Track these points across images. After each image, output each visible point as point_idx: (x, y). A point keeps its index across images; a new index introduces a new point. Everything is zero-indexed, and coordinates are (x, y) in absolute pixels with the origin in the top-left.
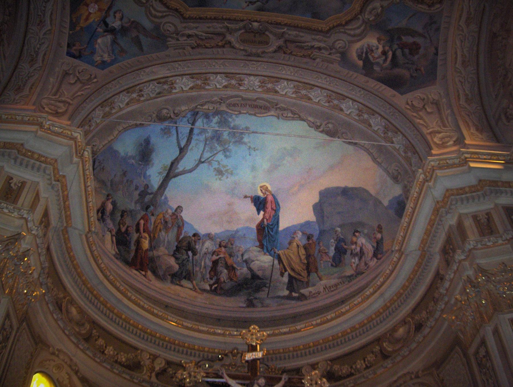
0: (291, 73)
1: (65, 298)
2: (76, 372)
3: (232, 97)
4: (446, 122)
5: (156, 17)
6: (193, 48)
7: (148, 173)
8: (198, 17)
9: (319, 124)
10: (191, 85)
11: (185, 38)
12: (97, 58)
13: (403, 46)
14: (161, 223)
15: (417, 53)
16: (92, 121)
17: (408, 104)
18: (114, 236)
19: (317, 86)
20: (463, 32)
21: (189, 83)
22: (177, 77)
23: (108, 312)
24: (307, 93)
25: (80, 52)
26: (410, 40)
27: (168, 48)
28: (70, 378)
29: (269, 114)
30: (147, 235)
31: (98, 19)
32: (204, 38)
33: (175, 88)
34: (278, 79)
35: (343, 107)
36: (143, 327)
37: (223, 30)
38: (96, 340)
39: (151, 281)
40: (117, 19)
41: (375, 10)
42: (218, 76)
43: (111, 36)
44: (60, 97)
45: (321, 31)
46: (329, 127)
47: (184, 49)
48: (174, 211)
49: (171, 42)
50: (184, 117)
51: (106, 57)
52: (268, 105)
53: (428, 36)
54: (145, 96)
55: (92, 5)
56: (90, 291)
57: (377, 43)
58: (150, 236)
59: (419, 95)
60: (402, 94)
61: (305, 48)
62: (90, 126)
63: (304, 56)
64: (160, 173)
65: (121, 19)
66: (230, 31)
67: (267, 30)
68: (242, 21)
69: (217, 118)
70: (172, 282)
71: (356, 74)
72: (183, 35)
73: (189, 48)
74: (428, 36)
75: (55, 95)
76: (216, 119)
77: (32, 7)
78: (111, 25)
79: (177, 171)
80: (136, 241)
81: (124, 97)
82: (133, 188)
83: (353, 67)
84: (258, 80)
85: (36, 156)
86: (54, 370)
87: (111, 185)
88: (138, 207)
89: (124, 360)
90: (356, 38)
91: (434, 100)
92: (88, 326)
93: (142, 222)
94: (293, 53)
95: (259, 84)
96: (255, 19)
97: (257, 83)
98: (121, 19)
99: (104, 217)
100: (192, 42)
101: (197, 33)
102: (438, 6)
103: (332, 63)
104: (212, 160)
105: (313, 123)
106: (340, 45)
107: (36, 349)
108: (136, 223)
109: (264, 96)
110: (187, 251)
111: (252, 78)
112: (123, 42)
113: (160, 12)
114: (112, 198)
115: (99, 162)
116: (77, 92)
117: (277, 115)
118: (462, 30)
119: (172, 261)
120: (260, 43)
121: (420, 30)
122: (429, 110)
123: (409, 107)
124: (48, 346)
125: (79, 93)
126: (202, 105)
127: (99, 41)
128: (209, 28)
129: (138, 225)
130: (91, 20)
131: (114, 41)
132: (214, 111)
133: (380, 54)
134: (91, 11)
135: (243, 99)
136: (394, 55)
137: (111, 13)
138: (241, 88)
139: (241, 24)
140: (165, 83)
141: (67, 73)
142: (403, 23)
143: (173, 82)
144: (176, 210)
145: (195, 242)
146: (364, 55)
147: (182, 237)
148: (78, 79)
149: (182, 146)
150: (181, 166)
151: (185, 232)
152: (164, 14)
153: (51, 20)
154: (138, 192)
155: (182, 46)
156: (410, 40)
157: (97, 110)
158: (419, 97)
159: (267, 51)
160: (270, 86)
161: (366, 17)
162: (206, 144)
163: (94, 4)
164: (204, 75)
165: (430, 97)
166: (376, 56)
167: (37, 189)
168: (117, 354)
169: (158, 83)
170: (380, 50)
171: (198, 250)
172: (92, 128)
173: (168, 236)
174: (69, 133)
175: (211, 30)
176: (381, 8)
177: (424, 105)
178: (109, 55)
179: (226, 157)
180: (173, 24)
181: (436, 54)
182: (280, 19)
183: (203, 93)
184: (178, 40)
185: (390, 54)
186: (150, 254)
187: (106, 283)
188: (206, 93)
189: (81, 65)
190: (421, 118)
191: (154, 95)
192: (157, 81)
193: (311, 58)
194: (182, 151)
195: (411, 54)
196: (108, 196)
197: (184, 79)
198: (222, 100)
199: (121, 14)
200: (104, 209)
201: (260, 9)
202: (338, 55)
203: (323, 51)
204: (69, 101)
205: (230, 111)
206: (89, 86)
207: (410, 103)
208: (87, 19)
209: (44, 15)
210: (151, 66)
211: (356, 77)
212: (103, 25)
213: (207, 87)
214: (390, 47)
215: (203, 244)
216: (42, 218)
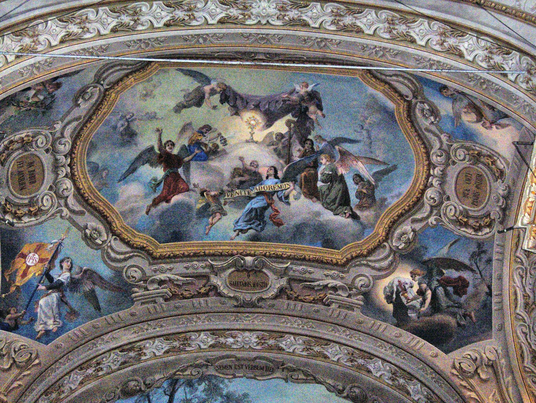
0: (299, 325)
3: (223, 357)
4: (506, 395)
5: (119, 261)
6: (166, 300)
8: (172, 255)
9: (341, 388)
10: (167, 348)
11: (156, 286)
12: (39, 327)
13: (445, 283)
15: (465, 293)
17: (454, 367)
19: (334, 342)
20: (523, 265)
24: (322, 350)
26: (453, 274)
27: (133, 302)
31: (40, 272)
33: (145, 354)
34: (282, 334)
35: (371, 367)
37: (207, 270)
41: (405, 236)
42: (202, 335)
43: (57, 294)
45: (337, 264)
46: (355, 392)
47: (155, 302)
49: (139, 292)
50: (158, 388)
51: (51, 326)
53: (476, 269)
54: (105, 369)
55: (31, 255)
57: (411, 278)
59: (469, 353)
60: (447, 352)
61: (316, 289)
63: (314, 301)
65: (70, 270)
66: (216, 272)
67: (264, 265)
68: (232, 255)
69: (204, 384)
71: (384, 325)
72: (153, 282)
73: (161, 300)
74: (476, 269)
76: (202, 386)
78: (56, 278)
81: (76, 376)
83: (379, 312)
84: (255, 336)
90: (383, 273)
91: (489, 360)
94: (300, 298)
95: (257, 340)
96: (248, 252)
97: (254, 339)
98: (70, 270)
100: (165, 290)
101: (172, 276)
102: (487, 230)
103: (353, 310)
105: (334, 387)
106: (362, 283)
109: (266, 354)
111: (247, 334)
113: (121, 253)
116: (13, 382)
117: (285, 377)
118: (522, 263)
120: (255, 285)
121: (467, 262)
122: (483, 376)
123: (455, 372)
125: (16, 384)
126: (182, 371)
127: (42, 302)
128: (187, 268)
130: (30, 276)
131: (62, 300)
133: (416, 294)
134: (29, 264)
135: (238, 359)
136: (434, 296)
137: (57, 262)
139: (230, 260)
140: (130, 350)
142: (443, 252)
146: (394, 296)
148: (14, 361)
155: (152, 297)
156: (453, 274)
158: (469, 357)
159: (265, 297)
160: (271, 342)
161: (394, 244)
163: (33, 254)
164: (183, 335)
165: (484, 356)
166: (410, 296)
169: (121, 351)
170: (416, 288)
175: (190, 271)
176: (412, 233)
177: (477, 368)
181: (490, 294)
182: (280, 251)
184: (146, 289)
185: (429, 294)
190: (472, 389)
192: (120, 349)
193: (324, 304)
195: (456, 292)
197: (156, 341)
198: (209, 362)
199: (69, 263)
201: (255, 238)
202: (361, 297)
203: (340, 292)
205: (221, 375)
206: (29, 372)
207: (457, 366)
208: (25, 274)
210: (111, 331)
211: (385, 328)
213: (188, 349)
214: (429, 285)
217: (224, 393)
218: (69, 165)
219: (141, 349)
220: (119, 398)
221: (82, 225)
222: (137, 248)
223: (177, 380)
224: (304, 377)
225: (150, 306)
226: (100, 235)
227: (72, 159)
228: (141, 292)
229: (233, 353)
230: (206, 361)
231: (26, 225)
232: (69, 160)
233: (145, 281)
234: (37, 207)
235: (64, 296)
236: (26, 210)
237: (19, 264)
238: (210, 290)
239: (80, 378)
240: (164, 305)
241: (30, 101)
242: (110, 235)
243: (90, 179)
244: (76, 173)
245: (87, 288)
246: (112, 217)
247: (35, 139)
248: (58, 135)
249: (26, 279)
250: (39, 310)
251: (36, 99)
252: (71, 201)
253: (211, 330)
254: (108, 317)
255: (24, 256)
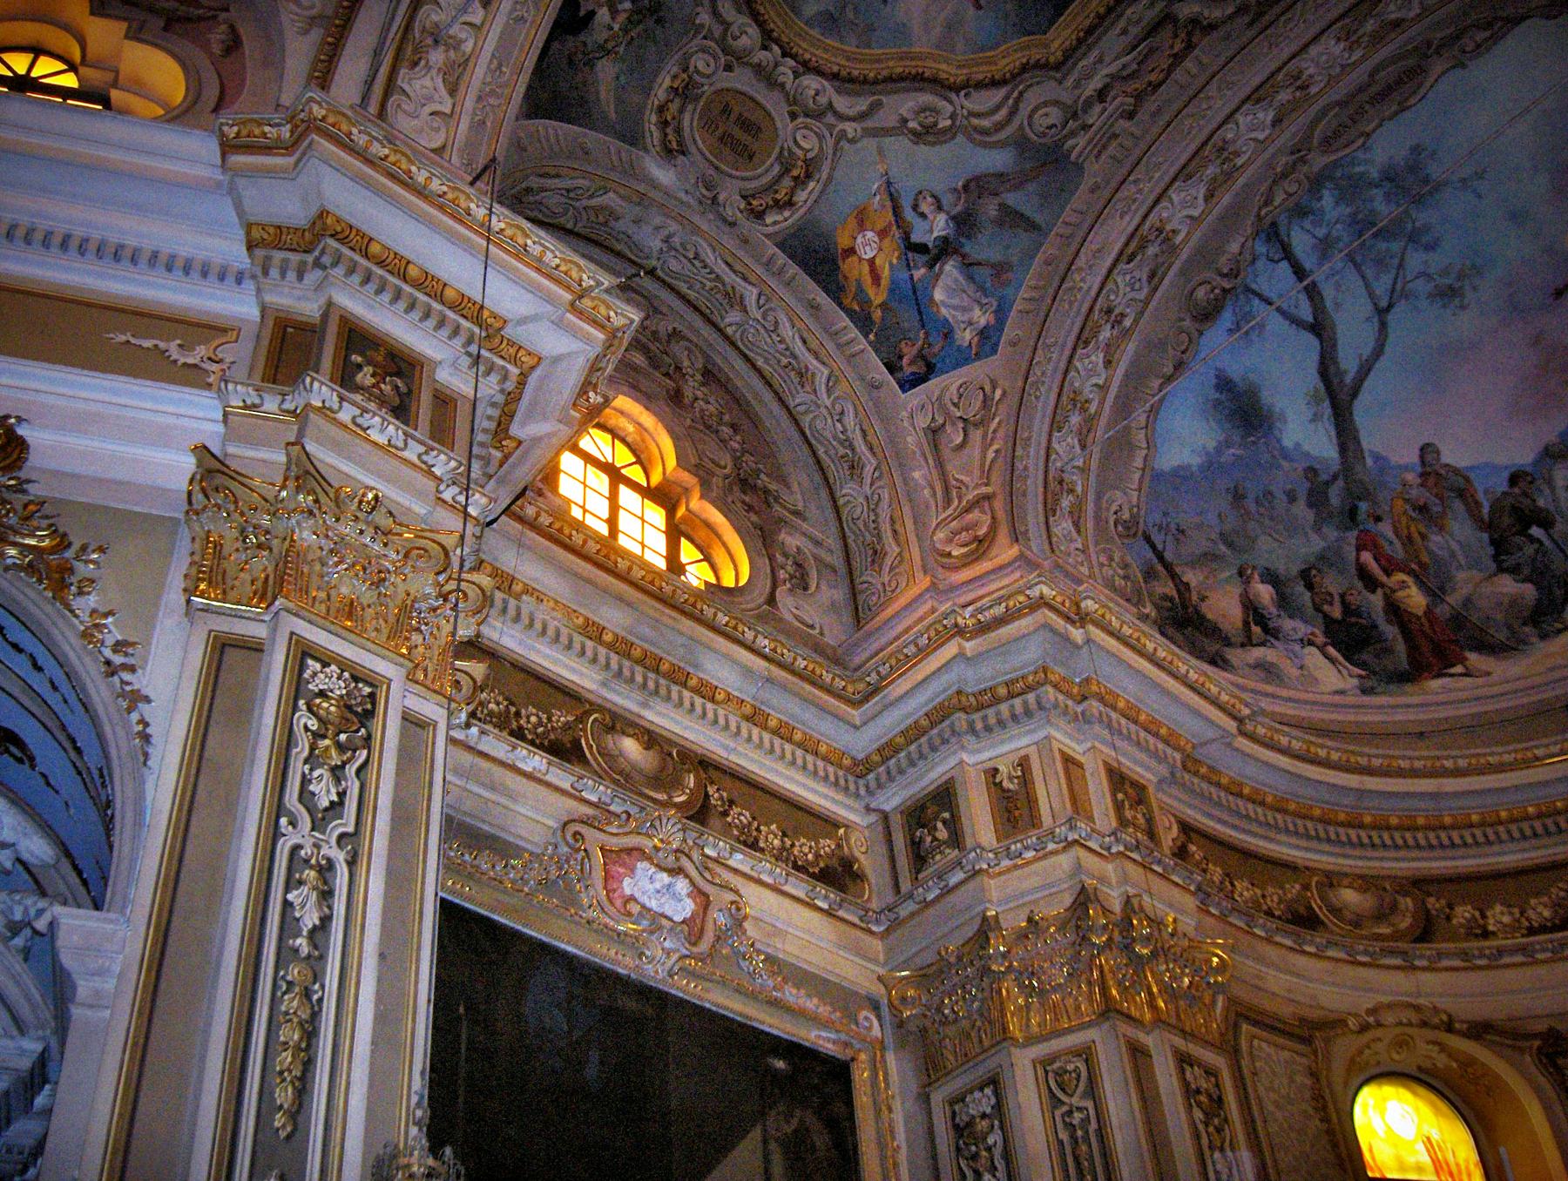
1: (1306, 887)
2: (1449, 1028)
5: (999, 127)
6: (1131, 115)
7: (1288, 442)
10: (1202, 191)
11: (1098, 108)
12: (966, 336)
14: (1413, 519)
16: (1066, 476)
18: (1326, 644)
21: (1193, 192)
22: (1157, 209)
23: (1432, 835)
25: (923, 358)
27: (1079, 168)
28: (1443, 1048)
29: (1432, 80)
30: (1402, 576)
32: (1135, 66)
36: (1538, 805)
38: (1448, 918)
39: (1488, 674)
40: (931, 217)
44: (960, 498)
47: (1115, 136)
48: (1420, 470)
50: (1254, 260)
51: (982, 318)
52: (1411, 62)
55: (859, 240)
56: (1354, 827)
58: (1410, 572)
62: (1071, 491)
64: (1316, 418)
65: (940, 208)
69: (1326, 193)
70: (1544, 637)
72: (1088, 104)
75: (948, 502)
76: (1327, 199)
77: (760, 363)
78: (929, 240)
79: (1348, 379)
80: (1386, 612)
82: (1281, 500)
85: (1002, 691)
86: (1396, 1057)
87: (1230, 545)
88: (1332, 533)
89: (1547, 913)
92: (1407, 903)
93: (1367, 557)
95: (1342, 45)
97: (1337, 49)
98: (940, 208)
99: (1271, 625)
100: (1118, 101)
101: (1113, 69)
104: (1405, 284)
107: (1315, 1053)
108: (1353, 571)
109: (1377, 58)
110: (1523, 532)
111: (1313, 51)
112: (984, 247)
113: (998, 108)
114: (1254, 568)
115: (1160, 530)
119: (1508, 586)
124: (1343, 1023)
125: (991, 455)
127: (938, 295)
128: (1124, 32)
129: (1363, 573)
130: (886, 273)
132: (1306, 185)
134: (870, 255)
137: (909, 214)
138: (1314, 90)
140: (1142, 247)
141: (934, 432)
143: (1158, 224)
144: (1423, 463)
145: (1525, 494)
147: (1485, 510)
148: (965, 420)
149: (1310, 319)
150: (1348, 362)
151: (1486, 492)
152: (1011, 101)
153: (816, 356)
154: (1301, 503)
157: (1055, 445)
162: (1357, 266)
167: (1057, 756)
168: (1522, 913)
171: (1552, 508)
172: (1079, 489)
173: (1451, 535)
174: (1021, 598)
175: (1135, 31)
178: (982, 306)
179: (1430, 247)
180: (1045, 104)
183: (1241, 181)
184: (1086, 127)
186: (1442, 611)
187: (1372, 783)
188: (1249, 173)
189: (946, 384)
191: (1145, 290)
192: (1124, 258)
194: (1319, 327)
196: (1241, 573)
197: (1174, 196)
198: (1299, 151)
199: (929, 199)
200: (1255, 610)
204: (984, 490)
205: (1341, 154)
209: (794, 357)
212: (917, 256)
213: (1240, 161)
215: (1550, 482)
216: (1114, 796)
217: (1375, 175)
218: (784, 55)
219: (1160, 231)
220: (1201, 333)
221: (892, 122)
222: (1014, 77)
223: (1274, 224)
224: (1487, 34)
225: (1111, 150)
226: (938, 112)
227: (777, 41)
228: (1081, 141)
229: (1321, 103)
230: (1292, 153)
231: (809, 203)
232: (776, 48)
233: (1075, 116)
234: (800, 163)
235: (964, 256)
236: (787, 183)
237: (854, 270)
238: (1189, 34)
239: (1099, 358)
240: (1133, 129)
241: (616, 27)
242: (953, 96)
243: (838, 45)
244: (807, 56)
245: (990, 209)
246: (930, 67)
247: (691, 69)
248: (717, 31)
249: (885, 282)
250: (944, 311)
251: (622, 17)
252: (841, 103)
253: (1249, 98)
254: (1059, 228)
255: (851, 251)
